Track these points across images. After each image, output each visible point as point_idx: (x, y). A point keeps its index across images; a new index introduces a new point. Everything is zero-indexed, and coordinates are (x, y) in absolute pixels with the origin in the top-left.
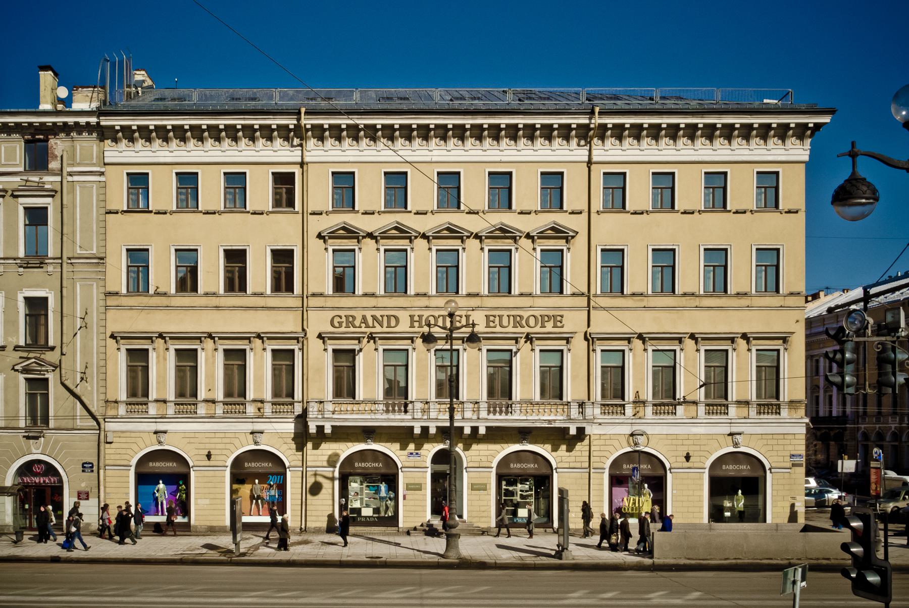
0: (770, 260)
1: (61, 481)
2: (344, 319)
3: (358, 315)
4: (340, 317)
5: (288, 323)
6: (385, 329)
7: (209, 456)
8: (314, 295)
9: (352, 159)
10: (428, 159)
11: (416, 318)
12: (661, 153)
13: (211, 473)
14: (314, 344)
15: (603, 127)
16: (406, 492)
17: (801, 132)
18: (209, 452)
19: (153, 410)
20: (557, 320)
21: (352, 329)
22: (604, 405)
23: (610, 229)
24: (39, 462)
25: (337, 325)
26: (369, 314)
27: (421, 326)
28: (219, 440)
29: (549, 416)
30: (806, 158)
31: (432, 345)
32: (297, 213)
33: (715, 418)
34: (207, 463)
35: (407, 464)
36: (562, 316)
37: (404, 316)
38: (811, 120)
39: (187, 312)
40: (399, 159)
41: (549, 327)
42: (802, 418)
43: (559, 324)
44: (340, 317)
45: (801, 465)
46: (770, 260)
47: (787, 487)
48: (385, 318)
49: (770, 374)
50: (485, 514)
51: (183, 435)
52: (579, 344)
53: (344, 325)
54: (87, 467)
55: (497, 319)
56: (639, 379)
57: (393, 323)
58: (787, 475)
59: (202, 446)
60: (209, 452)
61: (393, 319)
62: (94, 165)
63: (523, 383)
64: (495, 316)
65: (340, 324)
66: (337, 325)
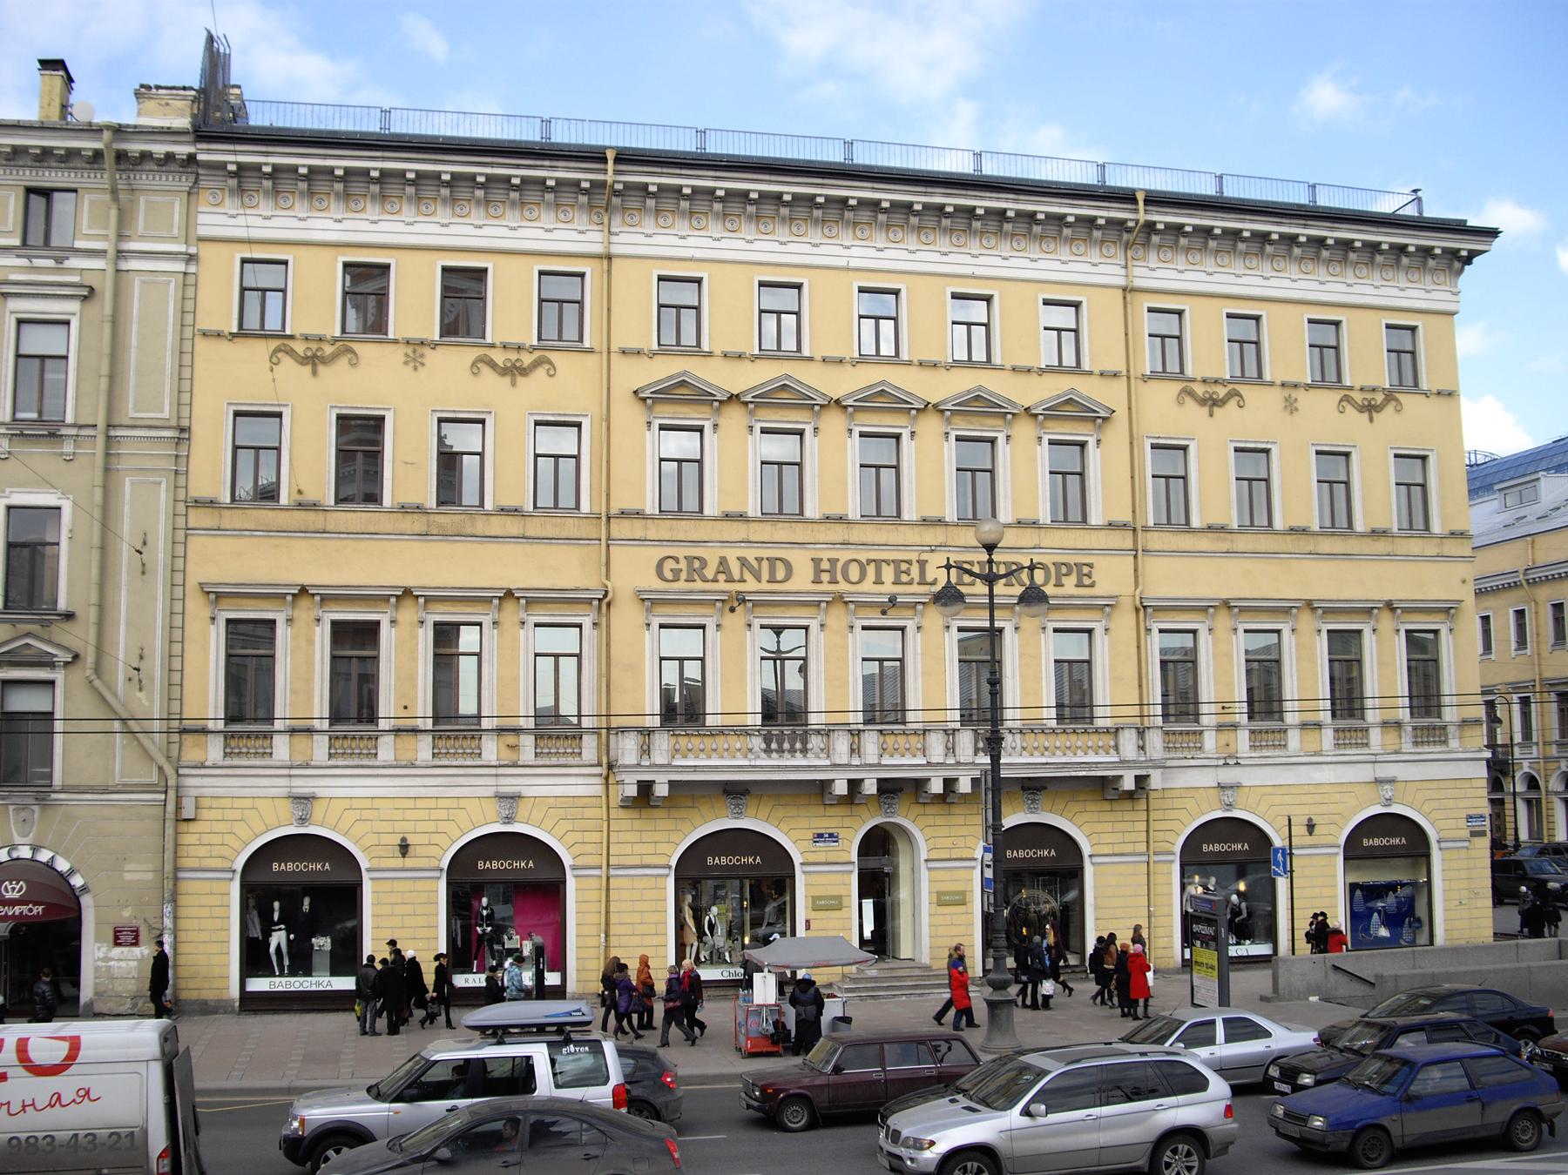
2: (683, 565)
3: (712, 556)
4: (677, 560)
6: (765, 586)
7: (404, 848)
8: (624, 514)
9: (698, 254)
10: (842, 262)
11: (825, 565)
12: (1239, 281)
13: (408, 885)
15: (1150, 227)
16: (813, 915)
18: (404, 839)
19: (282, 747)
20: (1083, 573)
21: (699, 585)
22: (1167, 733)
25: (669, 575)
26: (732, 555)
27: (833, 581)
28: (424, 814)
29: (1080, 755)
31: (953, 616)
33: (1352, 753)
34: (399, 862)
35: (812, 858)
36: (1090, 566)
37: (801, 562)
39: (363, 545)
41: (1070, 582)
42: (1480, 751)
43: (1086, 581)
44: (677, 560)
45: (1483, 834)
47: (1464, 874)
48: (765, 564)
50: (217, 912)
51: (347, 804)
52: (1125, 621)
53: (684, 575)
56: (1222, 680)
57: (780, 575)
58: (1463, 853)
59: (388, 827)
60: (404, 839)
61: (780, 567)
62: (173, 239)
63: (413, 678)
64: (909, 562)
65: (676, 573)
66: (669, 575)
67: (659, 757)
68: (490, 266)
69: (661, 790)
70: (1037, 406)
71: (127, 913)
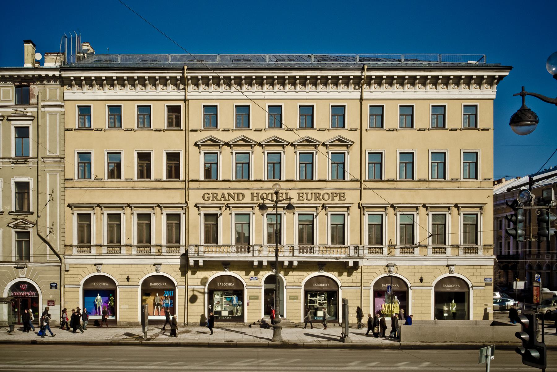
0: (472, 159)
1: (37, 294)
2: (211, 195)
3: (220, 193)
4: (209, 194)
5: (177, 198)
6: (236, 202)
7: (128, 279)
8: (192, 180)
9: (216, 97)
10: (262, 97)
11: (255, 195)
12: (405, 93)
13: (129, 290)
14: (193, 211)
15: (370, 78)
16: (249, 301)
17: (491, 81)
18: (128, 277)
19: (94, 251)
20: (341, 196)
21: (216, 201)
22: (370, 248)
23: (374, 140)
24: (24, 282)
25: (206, 199)
26: (226, 192)
27: (258, 200)
28: (134, 269)
29: (336, 255)
30: (494, 97)
31: (264, 211)
32: (182, 130)
33: (438, 256)
34: (127, 283)
35: (249, 284)
36: (344, 194)
37: (247, 193)
38: (497, 74)
39: (115, 191)
40: (244, 97)
41: (337, 200)
42: (491, 256)
43: (342, 198)
44: (209, 194)
45: (491, 285)
46: (472, 159)
47: (482, 298)
48: (236, 195)
49: (472, 229)
51: (112, 266)
52: (355, 210)
53: (211, 199)
54: (53, 286)
55: (305, 195)
56: (392, 232)
57: (241, 197)
58: (482, 291)
59: (124, 273)
60: (128, 277)
61: (241, 195)
62: (57, 101)
64: (303, 194)
65: (209, 198)
66: (206, 199)
67: (265, 254)
68: (446, 104)
69: (265, 264)
70: (263, 141)
71: (51, 297)
